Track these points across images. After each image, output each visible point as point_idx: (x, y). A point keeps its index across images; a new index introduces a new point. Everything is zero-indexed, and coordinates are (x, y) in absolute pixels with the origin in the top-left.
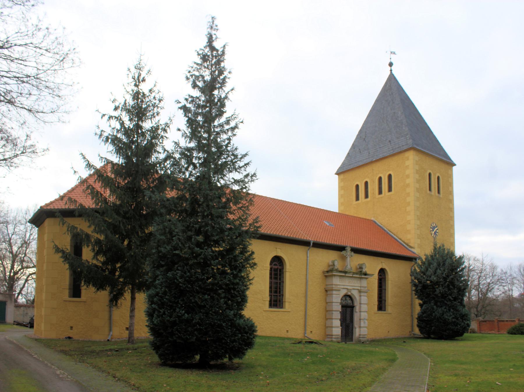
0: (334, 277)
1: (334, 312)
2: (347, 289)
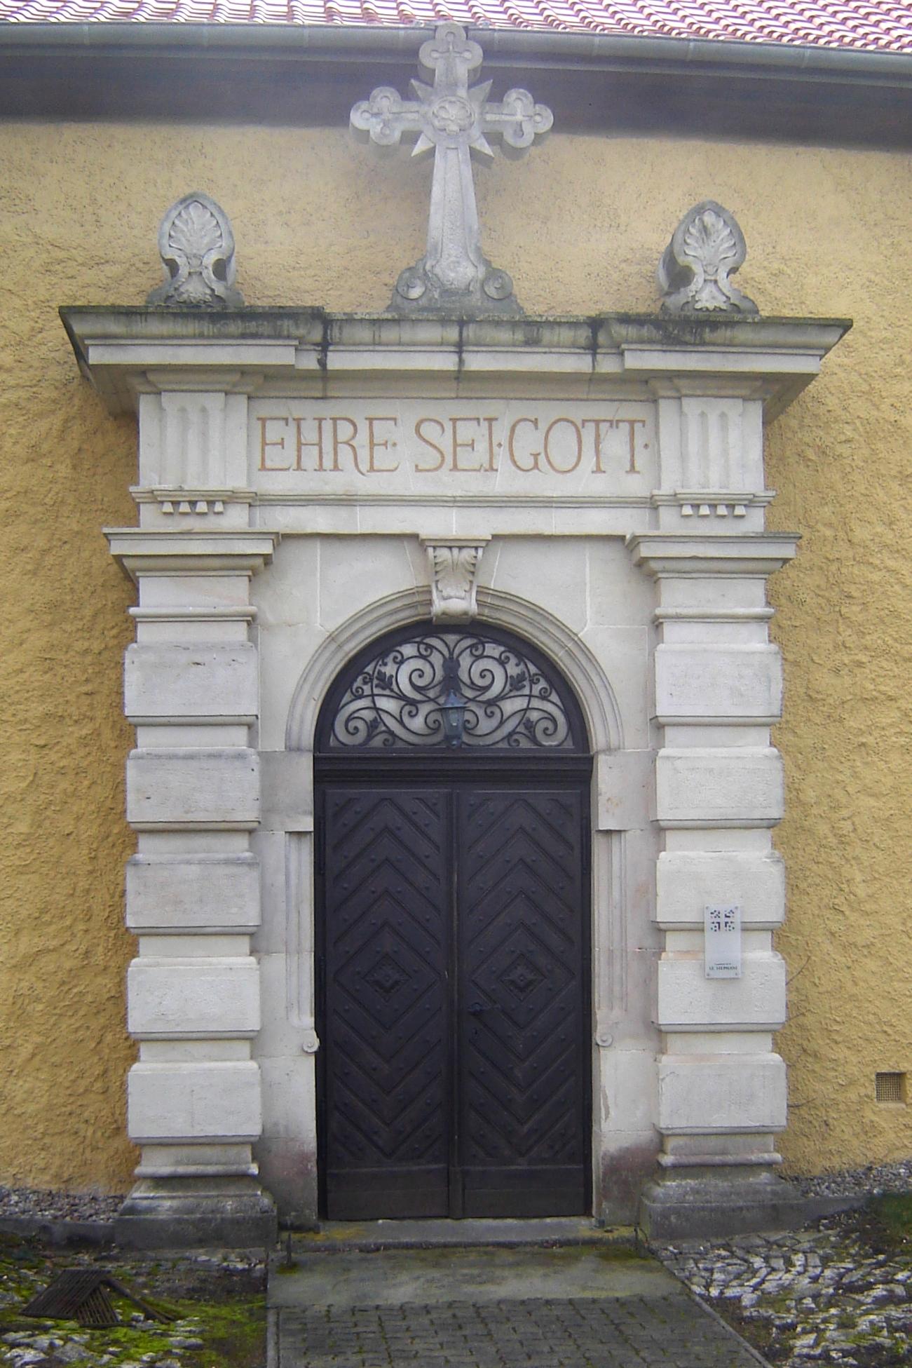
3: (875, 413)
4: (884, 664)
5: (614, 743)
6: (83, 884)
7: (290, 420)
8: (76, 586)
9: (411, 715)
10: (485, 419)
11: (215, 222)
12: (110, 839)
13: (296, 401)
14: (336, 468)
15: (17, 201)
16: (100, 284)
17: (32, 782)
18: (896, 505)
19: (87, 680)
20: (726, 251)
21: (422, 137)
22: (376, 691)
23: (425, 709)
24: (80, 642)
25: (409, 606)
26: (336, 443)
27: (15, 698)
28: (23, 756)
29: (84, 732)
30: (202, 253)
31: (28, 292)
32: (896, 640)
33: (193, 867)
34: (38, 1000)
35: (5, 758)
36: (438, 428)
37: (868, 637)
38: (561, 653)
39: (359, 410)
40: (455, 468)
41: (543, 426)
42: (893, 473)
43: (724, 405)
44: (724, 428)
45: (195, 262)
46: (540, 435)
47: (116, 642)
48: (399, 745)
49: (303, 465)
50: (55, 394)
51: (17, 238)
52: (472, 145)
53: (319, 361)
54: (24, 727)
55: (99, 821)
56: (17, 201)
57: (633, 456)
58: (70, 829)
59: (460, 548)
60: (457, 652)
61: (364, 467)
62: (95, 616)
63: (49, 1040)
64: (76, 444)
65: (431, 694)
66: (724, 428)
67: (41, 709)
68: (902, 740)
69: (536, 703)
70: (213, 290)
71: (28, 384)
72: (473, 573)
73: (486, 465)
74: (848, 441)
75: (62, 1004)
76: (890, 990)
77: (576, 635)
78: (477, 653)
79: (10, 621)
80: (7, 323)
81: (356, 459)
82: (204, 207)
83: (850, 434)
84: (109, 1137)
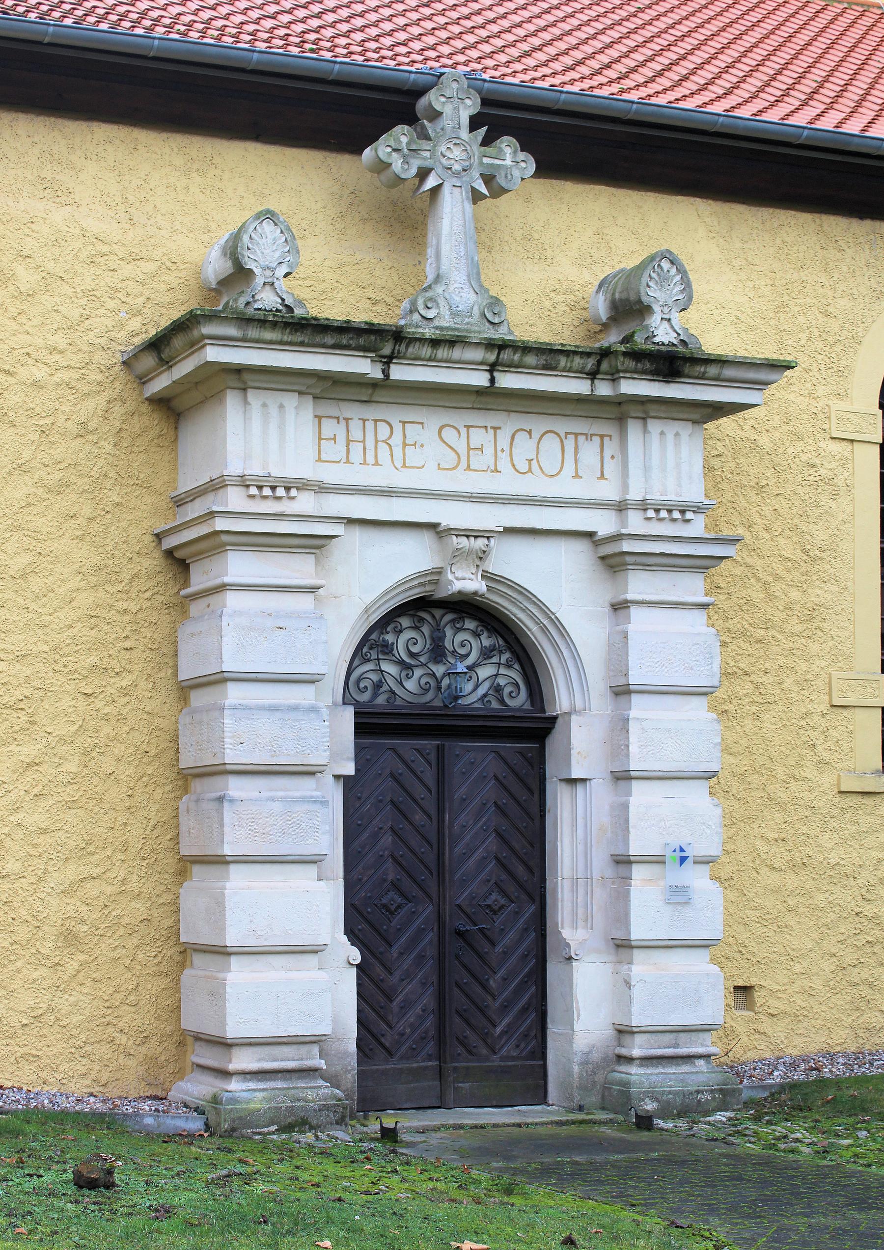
0: (232, 401)
1: (236, 787)
2: (432, 527)
3: (739, 432)
4: (742, 644)
5: (579, 705)
6: (121, 819)
7: (341, 419)
8: (117, 552)
9: (408, 677)
10: (492, 428)
11: (284, 239)
12: (144, 779)
13: (346, 403)
14: (376, 463)
15: (59, 193)
16: (138, 279)
17: (81, 726)
18: (753, 510)
19: (127, 637)
20: (676, 295)
21: (433, 173)
22: (381, 657)
23: (418, 672)
24: (121, 603)
25: (421, 585)
26: (377, 441)
27: (66, 650)
28: (73, 703)
29: (124, 683)
30: (274, 265)
31: (76, 281)
32: (750, 624)
33: (277, 804)
34: (83, 921)
35: (57, 705)
36: (455, 432)
37: (730, 621)
38: (535, 628)
39: (395, 415)
40: (468, 468)
41: (536, 435)
42: (753, 484)
43: (677, 426)
44: (677, 445)
45: (269, 273)
46: (532, 443)
47: (149, 603)
48: (399, 702)
49: (352, 460)
50: (100, 377)
51: (68, 229)
52: (473, 185)
53: (383, 371)
54: (73, 677)
55: (136, 762)
56: (59, 193)
57: (602, 466)
58: (112, 769)
59: (476, 537)
60: (442, 623)
61: (399, 464)
62: (132, 580)
63: (92, 958)
64: (117, 424)
65: (423, 659)
66: (677, 445)
67: (88, 661)
68: (754, 708)
69: (502, 671)
70: (283, 300)
71: (78, 365)
72: (481, 558)
73: (493, 468)
74: (719, 455)
75: (104, 926)
76: (744, 916)
77: (553, 614)
78: (458, 626)
79: (62, 581)
80: (59, 308)
81: (392, 456)
82: (276, 224)
83: (721, 449)
84: (139, 1045)
